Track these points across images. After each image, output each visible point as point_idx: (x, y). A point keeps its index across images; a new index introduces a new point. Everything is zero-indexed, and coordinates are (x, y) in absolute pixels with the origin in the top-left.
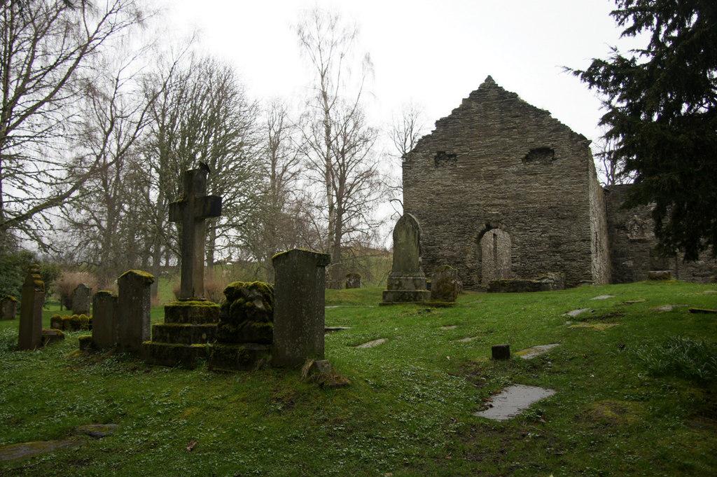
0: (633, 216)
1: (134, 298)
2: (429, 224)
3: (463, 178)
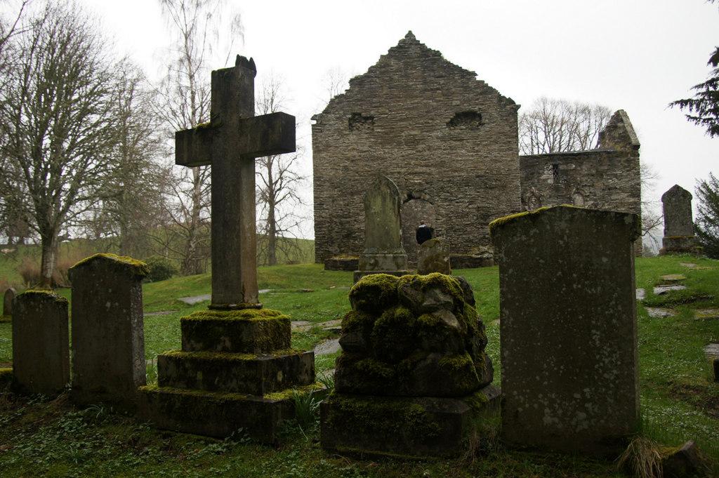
0: (531, 188)
1: (108, 304)
2: (343, 194)
3: (381, 143)
